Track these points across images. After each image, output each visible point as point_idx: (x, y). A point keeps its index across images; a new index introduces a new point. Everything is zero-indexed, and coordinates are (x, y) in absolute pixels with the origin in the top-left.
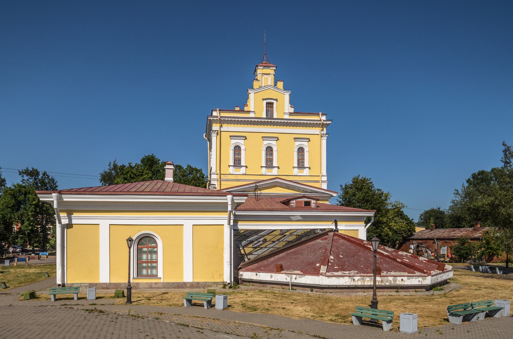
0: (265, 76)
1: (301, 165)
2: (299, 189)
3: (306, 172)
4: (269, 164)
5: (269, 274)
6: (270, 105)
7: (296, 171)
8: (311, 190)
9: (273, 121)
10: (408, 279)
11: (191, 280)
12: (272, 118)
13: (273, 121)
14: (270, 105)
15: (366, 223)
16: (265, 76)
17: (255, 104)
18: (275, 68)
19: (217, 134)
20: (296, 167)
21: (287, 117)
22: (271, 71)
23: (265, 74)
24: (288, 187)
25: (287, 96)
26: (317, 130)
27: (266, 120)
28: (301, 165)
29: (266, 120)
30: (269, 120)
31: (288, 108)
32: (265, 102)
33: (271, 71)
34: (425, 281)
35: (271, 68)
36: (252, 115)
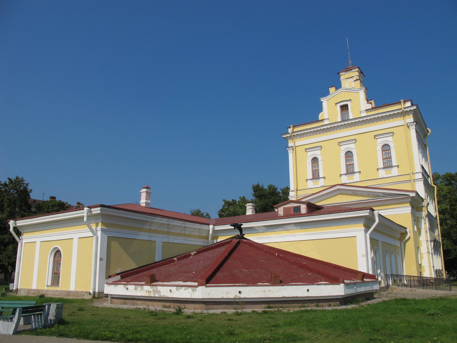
0: (350, 80)
1: (388, 165)
2: (368, 194)
3: (394, 171)
4: (350, 171)
5: (242, 296)
6: (345, 108)
7: (382, 173)
8: (384, 194)
9: (350, 122)
10: (177, 290)
11: (74, 290)
12: (349, 120)
13: (350, 122)
14: (345, 108)
15: (367, 227)
16: (350, 80)
17: (329, 110)
18: (357, 69)
19: (293, 149)
20: (380, 168)
21: (364, 114)
22: (355, 73)
23: (349, 78)
24: (354, 193)
25: (362, 94)
26: (399, 121)
27: (343, 124)
28: (388, 165)
29: (343, 124)
30: (346, 122)
31: (364, 105)
32: (338, 106)
33: (355, 73)
34: (195, 293)
35: (353, 70)
36: (326, 122)
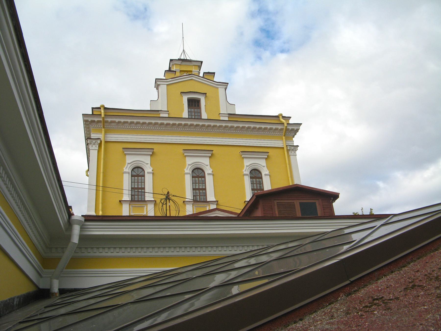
32: (185, 99)
